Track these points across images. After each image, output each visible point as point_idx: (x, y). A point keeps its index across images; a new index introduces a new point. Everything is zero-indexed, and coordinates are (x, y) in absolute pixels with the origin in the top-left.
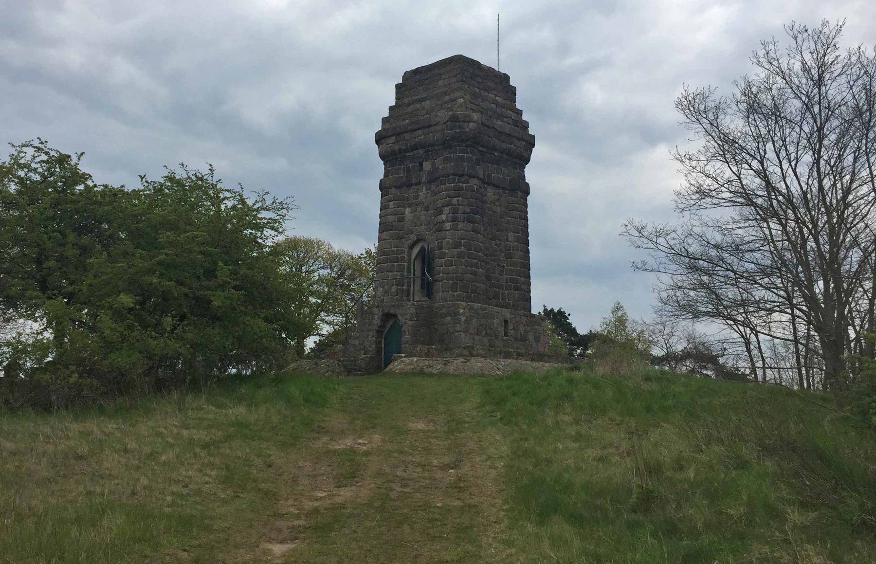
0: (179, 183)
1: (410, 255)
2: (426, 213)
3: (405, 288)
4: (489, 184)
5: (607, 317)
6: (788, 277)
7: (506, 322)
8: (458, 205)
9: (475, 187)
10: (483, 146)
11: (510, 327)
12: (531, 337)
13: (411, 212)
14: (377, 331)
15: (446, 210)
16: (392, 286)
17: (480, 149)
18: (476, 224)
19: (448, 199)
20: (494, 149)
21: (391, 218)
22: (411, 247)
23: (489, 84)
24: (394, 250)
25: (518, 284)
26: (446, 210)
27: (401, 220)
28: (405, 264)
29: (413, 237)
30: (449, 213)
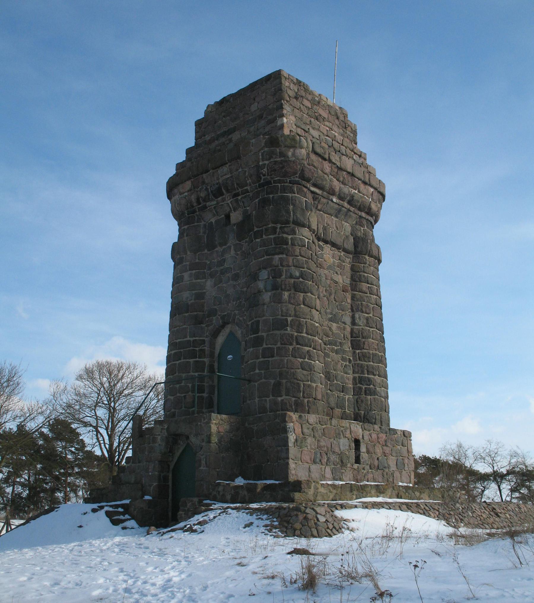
0: (455, 463)
1: (212, 345)
2: (235, 283)
3: (205, 395)
4: (326, 242)
5: (147, 370)
6: (56, 401)
7: (357, 442)
8: (282, 265)
9: (307, 240)
10: (315, 185)
11: (363, 449)
12: (392, 462)
13: (215, 285)
14: (160, 462)
15: (264, 274)
16: (188, 392)
17: (313, 189)
18: (309, 294)
19: (265, 257)
20: (332, 192)
21: (186, 295)
22: (215, 334)
23: (321, 112)
24: (190, 341)
25: (372, 386)
26: (264, 274)
27: (200, 296)
28: (205, 360)
29: (216, 321)
30: (269, 278)
